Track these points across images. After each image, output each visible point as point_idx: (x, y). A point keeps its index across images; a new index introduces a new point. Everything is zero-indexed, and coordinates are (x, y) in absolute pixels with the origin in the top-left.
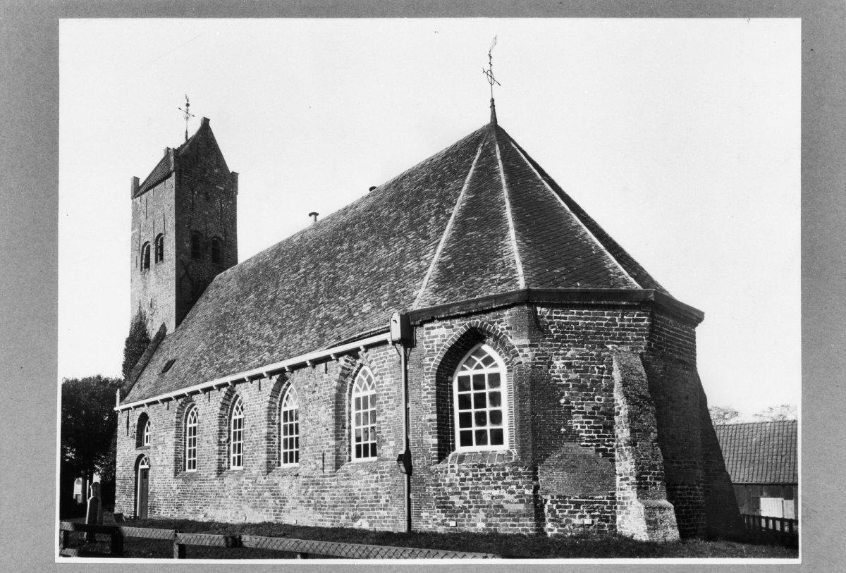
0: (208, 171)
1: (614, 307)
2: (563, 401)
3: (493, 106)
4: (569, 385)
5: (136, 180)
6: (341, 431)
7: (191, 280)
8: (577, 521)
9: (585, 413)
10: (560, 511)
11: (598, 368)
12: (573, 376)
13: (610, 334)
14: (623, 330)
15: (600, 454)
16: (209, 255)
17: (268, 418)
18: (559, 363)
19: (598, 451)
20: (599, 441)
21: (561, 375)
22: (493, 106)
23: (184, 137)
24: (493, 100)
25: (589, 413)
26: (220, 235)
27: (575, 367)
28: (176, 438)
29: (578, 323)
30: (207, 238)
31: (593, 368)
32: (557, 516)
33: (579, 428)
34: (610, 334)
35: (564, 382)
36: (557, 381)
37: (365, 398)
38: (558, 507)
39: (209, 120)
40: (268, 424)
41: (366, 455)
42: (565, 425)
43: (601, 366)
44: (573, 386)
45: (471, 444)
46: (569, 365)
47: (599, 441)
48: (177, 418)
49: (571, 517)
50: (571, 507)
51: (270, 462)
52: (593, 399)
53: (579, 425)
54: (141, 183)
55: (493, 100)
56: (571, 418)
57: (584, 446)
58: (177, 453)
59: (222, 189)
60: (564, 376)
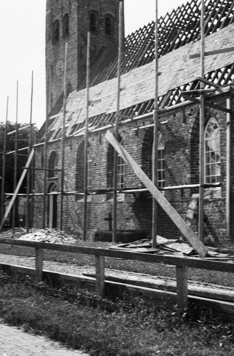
6: (195, 167)
16: (102, 29)
26: (110, 13)
30: (101, 16)
40: (143, 161)
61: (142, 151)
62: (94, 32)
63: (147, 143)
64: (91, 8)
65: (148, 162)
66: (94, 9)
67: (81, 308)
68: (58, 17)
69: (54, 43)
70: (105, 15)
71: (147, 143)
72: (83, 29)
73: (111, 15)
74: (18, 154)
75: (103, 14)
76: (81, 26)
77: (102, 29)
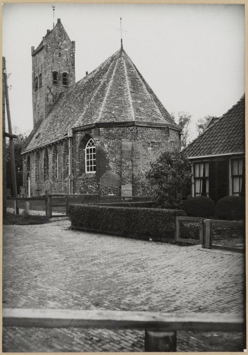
0: (60, 43)
1: (124, 127)
2: (107, 158)
3: (122, 41)
4: (109, 153)
5: (33, 48)
6: (65, 166)
7: (52, 94)
8: (109, 195)
9: (113, 161)
10: (105, 192)
11: (117, 147)
12: (110, 149)
13: (123, 136)
14: (127, 134)
15: (117, 174)
16: (61, 82)
17: (53, 160)
18: (106, 146)
19: (116, 173)
20: (117, 170)
21: (106, 149)
22: (122, 41)
23: (53, 27)
24: (122, 39)
25: (114, 161)
26: (66, 72)
27: (110, 147)
28: (36, 166)
29: (113, 133)
30: (60, 74)
31: (116, 147)
32: (104, 193)
33: (111, 166)
34: (123, 136)
35: (107, 152)
36: (106, 151)
37: (91, 149)
38: (105, 190)
39: (60, 19)
40: (53, 163)
41: (91, 170)
42: (107, 165)
43: (118, 146)
44: (110, 153)
45: (92, 171)
46: (109, 146)
47: (117, 170)
48: (36, 158)
49: (108, 193)
50: (108, 190)
51: (54, 176)
52: (115, 157)
53: (111, 165)
54: (35, 49)
55: (122, 39)
56: (109, 163)
57: (112, 171)
58: (36, 173)
59: (68, 50)
60: (107, 150)
61: (53, 158)
62: (56, 85)
63: (55, 154)
64: (53, 70)
65: (56, 163)
66: (55, 71)
67: (231, 339)
68: (37, 75)
69: (36, 91)
70: (63, 74)
71: (55, 154)
72: (48, 84)
73: (66, 73)
74: (89, 149)
75: (61, 73)
76: (48, 82)
77: (61, 82)
